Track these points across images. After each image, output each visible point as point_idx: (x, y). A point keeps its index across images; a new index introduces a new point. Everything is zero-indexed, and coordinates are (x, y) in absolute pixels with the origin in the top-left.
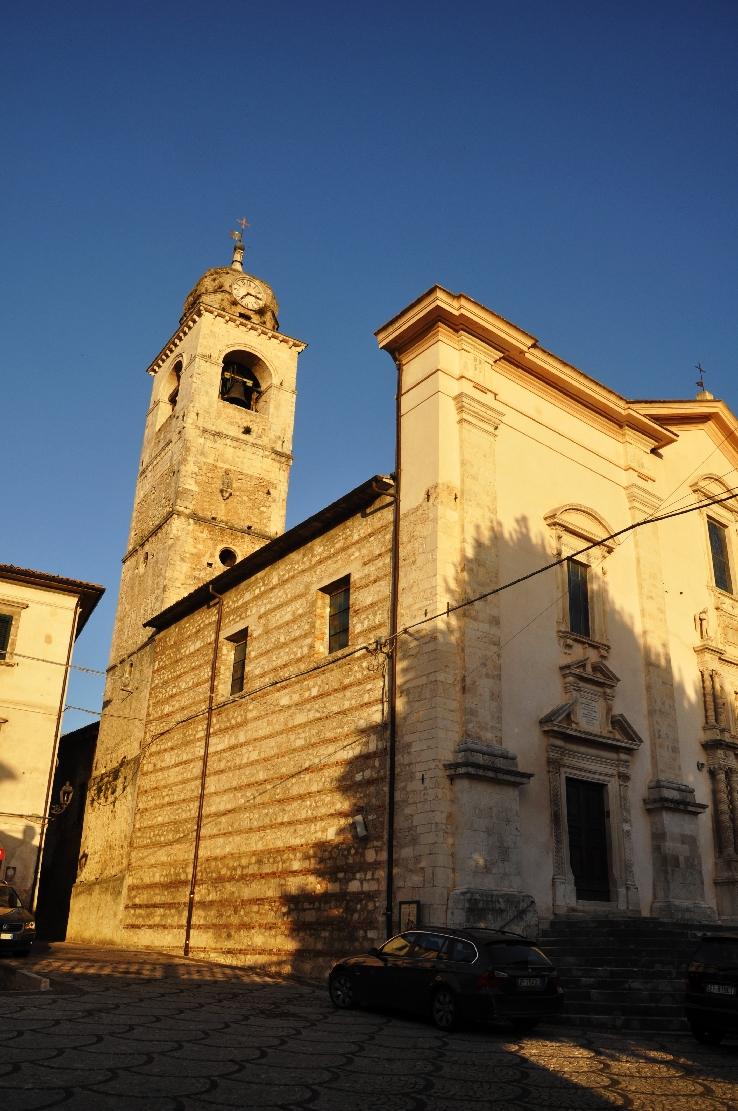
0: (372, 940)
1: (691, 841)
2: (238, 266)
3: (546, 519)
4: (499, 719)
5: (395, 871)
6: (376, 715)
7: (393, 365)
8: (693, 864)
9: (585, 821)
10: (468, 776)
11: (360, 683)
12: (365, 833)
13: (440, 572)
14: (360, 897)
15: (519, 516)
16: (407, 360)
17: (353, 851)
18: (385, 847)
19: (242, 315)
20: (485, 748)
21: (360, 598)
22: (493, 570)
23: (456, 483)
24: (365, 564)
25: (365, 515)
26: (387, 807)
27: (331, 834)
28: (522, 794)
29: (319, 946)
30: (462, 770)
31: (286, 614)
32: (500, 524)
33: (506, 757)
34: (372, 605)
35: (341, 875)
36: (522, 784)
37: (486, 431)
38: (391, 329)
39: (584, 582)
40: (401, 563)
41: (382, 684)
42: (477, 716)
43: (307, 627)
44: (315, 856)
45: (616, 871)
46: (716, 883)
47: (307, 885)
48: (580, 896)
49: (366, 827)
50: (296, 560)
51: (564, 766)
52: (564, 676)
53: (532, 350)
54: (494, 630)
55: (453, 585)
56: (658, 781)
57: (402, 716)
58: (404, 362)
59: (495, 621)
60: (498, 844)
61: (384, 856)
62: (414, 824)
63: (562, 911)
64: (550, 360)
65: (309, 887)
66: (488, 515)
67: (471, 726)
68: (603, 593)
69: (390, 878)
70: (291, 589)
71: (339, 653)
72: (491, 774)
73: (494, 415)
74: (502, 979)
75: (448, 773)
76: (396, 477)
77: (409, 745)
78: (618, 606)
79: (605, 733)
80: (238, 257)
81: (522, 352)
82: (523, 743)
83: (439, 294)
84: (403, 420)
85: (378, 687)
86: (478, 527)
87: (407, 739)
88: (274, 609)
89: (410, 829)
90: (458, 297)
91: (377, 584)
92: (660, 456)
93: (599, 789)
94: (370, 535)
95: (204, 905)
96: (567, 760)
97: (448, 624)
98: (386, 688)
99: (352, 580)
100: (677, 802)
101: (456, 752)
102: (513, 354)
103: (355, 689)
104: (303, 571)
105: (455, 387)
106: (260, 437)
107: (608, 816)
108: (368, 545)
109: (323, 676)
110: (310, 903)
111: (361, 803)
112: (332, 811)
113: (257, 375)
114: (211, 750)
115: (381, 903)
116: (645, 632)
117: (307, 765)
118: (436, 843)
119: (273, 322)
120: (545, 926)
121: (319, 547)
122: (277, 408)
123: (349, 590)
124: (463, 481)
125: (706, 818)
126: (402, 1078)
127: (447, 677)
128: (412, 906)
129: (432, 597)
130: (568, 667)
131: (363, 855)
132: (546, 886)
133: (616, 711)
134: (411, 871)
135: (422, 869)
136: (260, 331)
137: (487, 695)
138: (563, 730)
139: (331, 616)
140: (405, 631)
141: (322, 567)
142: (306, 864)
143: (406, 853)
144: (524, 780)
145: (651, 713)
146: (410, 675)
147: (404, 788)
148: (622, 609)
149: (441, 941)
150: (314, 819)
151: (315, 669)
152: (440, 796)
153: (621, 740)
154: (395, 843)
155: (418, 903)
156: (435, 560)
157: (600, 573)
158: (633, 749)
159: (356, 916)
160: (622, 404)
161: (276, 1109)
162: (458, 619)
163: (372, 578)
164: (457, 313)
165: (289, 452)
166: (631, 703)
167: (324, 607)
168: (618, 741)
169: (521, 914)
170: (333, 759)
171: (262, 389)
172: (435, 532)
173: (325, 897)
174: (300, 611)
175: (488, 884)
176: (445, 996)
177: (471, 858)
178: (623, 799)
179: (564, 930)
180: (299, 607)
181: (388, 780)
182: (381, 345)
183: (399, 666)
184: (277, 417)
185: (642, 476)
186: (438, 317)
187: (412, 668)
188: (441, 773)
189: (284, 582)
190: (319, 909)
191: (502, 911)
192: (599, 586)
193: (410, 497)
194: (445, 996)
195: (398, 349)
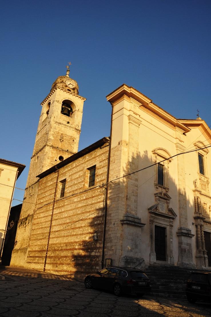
0: (98, 269)
1: (189, 245)
2: (68, 76)
3: (152, 151)
4: (137, 208)
5: (105, 250)
6: (101, 205)
7: (111, 106)
9: (160, 238)
10: (127, 224)
11: (97, 196)
12: (97, 239)
15: (145, 151)
17: (93, 244)
18: (103, 243)
19: (68, 90)
21: (98, 172)
22: (136, 166)
23: (127, 140)
24: (100, 162)
25: (101, 148)
27: (87, 239)
29: (82, 270)
30: (125, 222)
31: (77, 176)
32: (139, 152)
33: (138, 219)
35: (89, 250)
38: (111, 96)
39: (162, 170)
42: (130, 207)
43: (83, 179)
45: (168, 253)
46: (196, 257)
47: (80, 253)
48: (157, 260)
50: (81, 160)
52: (156, 196)
54: (136, 183)
55: (125, 169)
56: (181, 227)
59: (137, 180)
61: (102, 245)
63: (152, 263)
64: (155, 107)
65: (80, 254)
67: (128, 210)
68: (168, 174)
69: (103, 252)
70: (79, 168)
71: (92, 187)
72: (133, 223)
76: (110, 138)
80: (68, 73)
81: (148, 104)
82: (143, 215)
83: (125, 86)
84: (113, 122)
85: (103, 197)
86: (133, 153)
87: (110, 212)
89: (110, 238)
90: (130, 87)
92: (186, 135)
93: (164, 229)
94: (102, 154)
95: (50, 257)
96: (155, 220)
97: (123, 180)
99: (96, 166)
101: (124, 217)
105: (128, 113)
107: (166, 237)
108: (101, 157)
112: (88, 232)
114: (54, 213)
115: (101, 259)
117: (81, 219)
120: (147, 267)
121: (87, 157)
122: (77, 117)
124: (129, 140)
125: (194, 238)
127: (123, 195)
129: (119, 172)
130: (157, 194)
131: (96, 245)
132: (148, 256)
133: (170, 207)
134: (110, 250)
138: (154, 212)
140: (111, 182)
141: (88, 162)
142: (80, 247)
143: (108, 245)
144: (143, 226)
145: (180, 208)
147: (109, 226)
149: (117, 270)
151: (84, 191)
153: (171, 215)
154: (105, 242)
155: (111, 259)
156: (120, 162)
158: (174, 218)
159: (93, 262)
160: (175, 120)
162: (126, 179)
164: (130, 92)
165: (80, 129)
166: (174, 205)
168: (171, 216)
169: (140, 264)
170: (89, 217)
171: (73, 111)
172: (120, 154)
173: (85, 256)
174: (81, 175)
175: (131, 254)
178: (171, 232)
179: (152, 269)
180: (81, 173)
181: (104, 224)
182: (108, 100)
183: (109, 191)
186: (124, 93)
188: (119, 223)
189: (77, 166)
190: (83, 260)
195: (112, 101)
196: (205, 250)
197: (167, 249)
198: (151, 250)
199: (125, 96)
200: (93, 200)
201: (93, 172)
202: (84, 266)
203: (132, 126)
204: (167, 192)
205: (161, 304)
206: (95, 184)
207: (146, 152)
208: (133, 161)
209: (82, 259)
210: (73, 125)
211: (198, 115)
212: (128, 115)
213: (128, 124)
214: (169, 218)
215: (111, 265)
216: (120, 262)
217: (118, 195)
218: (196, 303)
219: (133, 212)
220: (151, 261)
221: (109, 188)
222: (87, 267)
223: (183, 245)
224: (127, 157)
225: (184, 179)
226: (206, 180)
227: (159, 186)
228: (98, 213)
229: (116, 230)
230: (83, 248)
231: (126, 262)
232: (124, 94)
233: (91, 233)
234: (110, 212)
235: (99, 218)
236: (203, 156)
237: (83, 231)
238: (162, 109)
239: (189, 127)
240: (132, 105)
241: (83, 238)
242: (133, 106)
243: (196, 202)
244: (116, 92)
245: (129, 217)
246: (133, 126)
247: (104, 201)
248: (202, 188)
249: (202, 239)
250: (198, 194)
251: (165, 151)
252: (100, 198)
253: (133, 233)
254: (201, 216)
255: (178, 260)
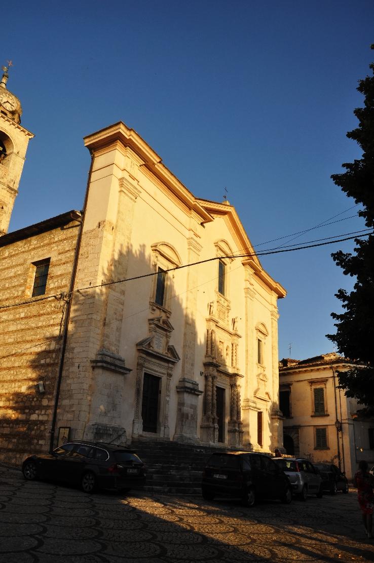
0: (41, 445)
1: (194, 407)
2: (4, 85)
3: (152, 247)
4: (119, 341)
5: (58, 411)
6: (56, 331)
7: (90, 157)
8: (194, 417)
9: (150, 394)
10: (103, 368)
11: (48, 314)
12: (44, 390)
13: (100, 265)
14: (35, 423)
15: (142, 244)
16: (98, 155)
17: (35, 399)
18: (54, 399)
19: (2, 112)
20: (111, 355)
21: (54, 271)
22: (125, 268)
23: (114, 222)
24: (60, 254)
25: (63, 229)
26: (58, 379)
27: (24, 389)
28: (125, 379)
29: (10, 446)
30: (99, 364)
31: (11, 273)
32: (131, 245)
33: (120, 360)
34: (61, 275)
35: (27, 411)
36: (126, 374)
37: (132, 199)
38: (92, 138)
39: (164, 280)
40: (80, 257)
41: (61, 316)
42: (109, 338)
43: (22, 281)
44: (13, 400)
45: (161, 419)
46: (201, 427)
47: (6, 414)
48: (144, 430)
49: (44, 387)
50: (20, 245)
51: (144, 367)
52: (150, 324)
53: (159, 164)
54: (122, 297)
55: (106, 272)
56: (184, 379)
57: (71, 333)
58: (96, 156)
59: (123, 293)
60: (112, 402)
61: (53, 403)
62: (72, 388)
63: (136, 436)
64: (166, 171)
65: (8, 416)
66: (127, 240)
67: (106, 343)
68: (171, 287)
69: (55, 414)
70: (15, 260)
71: (39, 297)
72: (113, 368)
73: (136, 191)
74: (120, 468)
75: (92, 365)
76: (83, 213)
77: (73, 349)
78: (177, 294)
79: (164, 354)
80: (4, 80)
81: (154, 164)
82: (128, 354)
83: (122, 126)
84: (91, 185)
85: (59, 317)
86: (122, 245)
87: (72, 345)
88: (4, 269)
89: (69, 391)
90: (130, 130)
91: (65, 265)
92: (204, 227)
93: (157, 380)
94: (64, 240)
96: (146, 365)
97: (101, 291)
98: (64, 318)
99: (51, 260)
100: (192, 389)
101: (97, 355)
102: (149, 164)
103: (46, 316)
104: (23, 252)
105: (120, 174)
106: (3, 178)
107: (160, 393)
108: (63, 244)
109: (28, 308)
110: (7, 424)
111: (43, 375)
112: (25, 378)
113: (6, 146)
115: (49, 426)
116: (187, 308)
117: (13, 353)
118: (82, 399)
119: (18, 120)
120: (129, 443)
121: (34, 241)
122: (14, 165)
123: (49, 265)
124: (117, 221)
125: (201, 397)
126: (83, 519)
127: (98, 317)
128: (66, 429)
129: (94, 276)
130: (152, 320)
131: (41, 401)
132: (130, 424)
133: (170, 344)
134: (67, 412)
135: (74, 411)
136: (11, 123)
137: (115, 328)
138: (146, 350)
139: (36, 278)
140: (78, 291)
141: (35, 251)
142: (7, 404)
143: (65, 402)
144: (128, 372)
145: (184, 346)
146: (77, 314)
147: (68, 370)
148: (179, 295)
149: (87, 448)
150: (14, 381)
151: (24, 303)
152: (87, 376)
153: (170, 358)
154: (60, 397)
155: (70, 428)
156: (98, 258)
157: (172, 277)
158: (175, 362)
159: (33, 432)
160: (193, 198)
161: (301, 562)
162: (106, 289)
163: (63, 262)
164: (128, 138)
165: (16, 189)
166: (177, 340)
167: (33, 273)
168: (170, 358)
169: (119, 437)
170: (29, 351)
171: (7, 153)
172: (101, 244)
173: (17, 422)
174: (19, 272)
175: (105, 421)
176: (89, 476)
177: (99, 408)
178: (168, 385)
179: (137, 445)
180: (20, 270)
181: (59, 365)
182: (86, 145)
183: (73, 308)
184: (14, 169)
185: (195, 234)
186: (118, 137)
187: (78, 310)
188: (89, 364)
189: (11, 256)
190: (12, 427)
191: (111, 435)
192: (171, 283)
193: (89, 224)
194: (89, 476)
195: (94, 149)
196: (216, 417)
197: (159, 412)
198: (136, 412)
199: (119, 144)
200: (40, 319)
201: (43, 269)
202: (15, 438)
203: (124, 197)
204: (168, 317)
205: (165, 505)
206: (46, 293)
207: (143, 247)
208: (119, 258)
209: (11, 425)
210: (5, 179)
211: (225, 197)
212: (120, 177)
213: (118, 194)
214: (168, 361)
215: (69, 439)
216: (85, 433)
217: (90, 316)
218: (214, 499)
219: (113, 348)
220: (135, 432)
221: (73, 302)
222: (21, 441)
223: (185, 408)
224: (110, 252)
225: (195, 299)
226: (226, 304)
227: (157, 307)
228: (49, 345)
229: (81, 378)
230: (14, 405)
231: (96, 433)
232: (116, 140)
233: (30, 379)
234: (71, 344)
235: (50, 355)
236: (226, 265)
237: (17, 374)
238: (175, 177)
239: (212, 215)
240: (128, 161)
241: (15, 387)
242: (129, 164)
243: (209, 339)
244: (105, 133)
245: (107, 355)
246: (126, 197)
247: (61, 323)
248: (220, 318)
249: (212, 399)
250: (212, 326)
251: (173, 250)
252: (54, 319)
253: (110, 384)
254: (214, 361)
255: (175, 432)
